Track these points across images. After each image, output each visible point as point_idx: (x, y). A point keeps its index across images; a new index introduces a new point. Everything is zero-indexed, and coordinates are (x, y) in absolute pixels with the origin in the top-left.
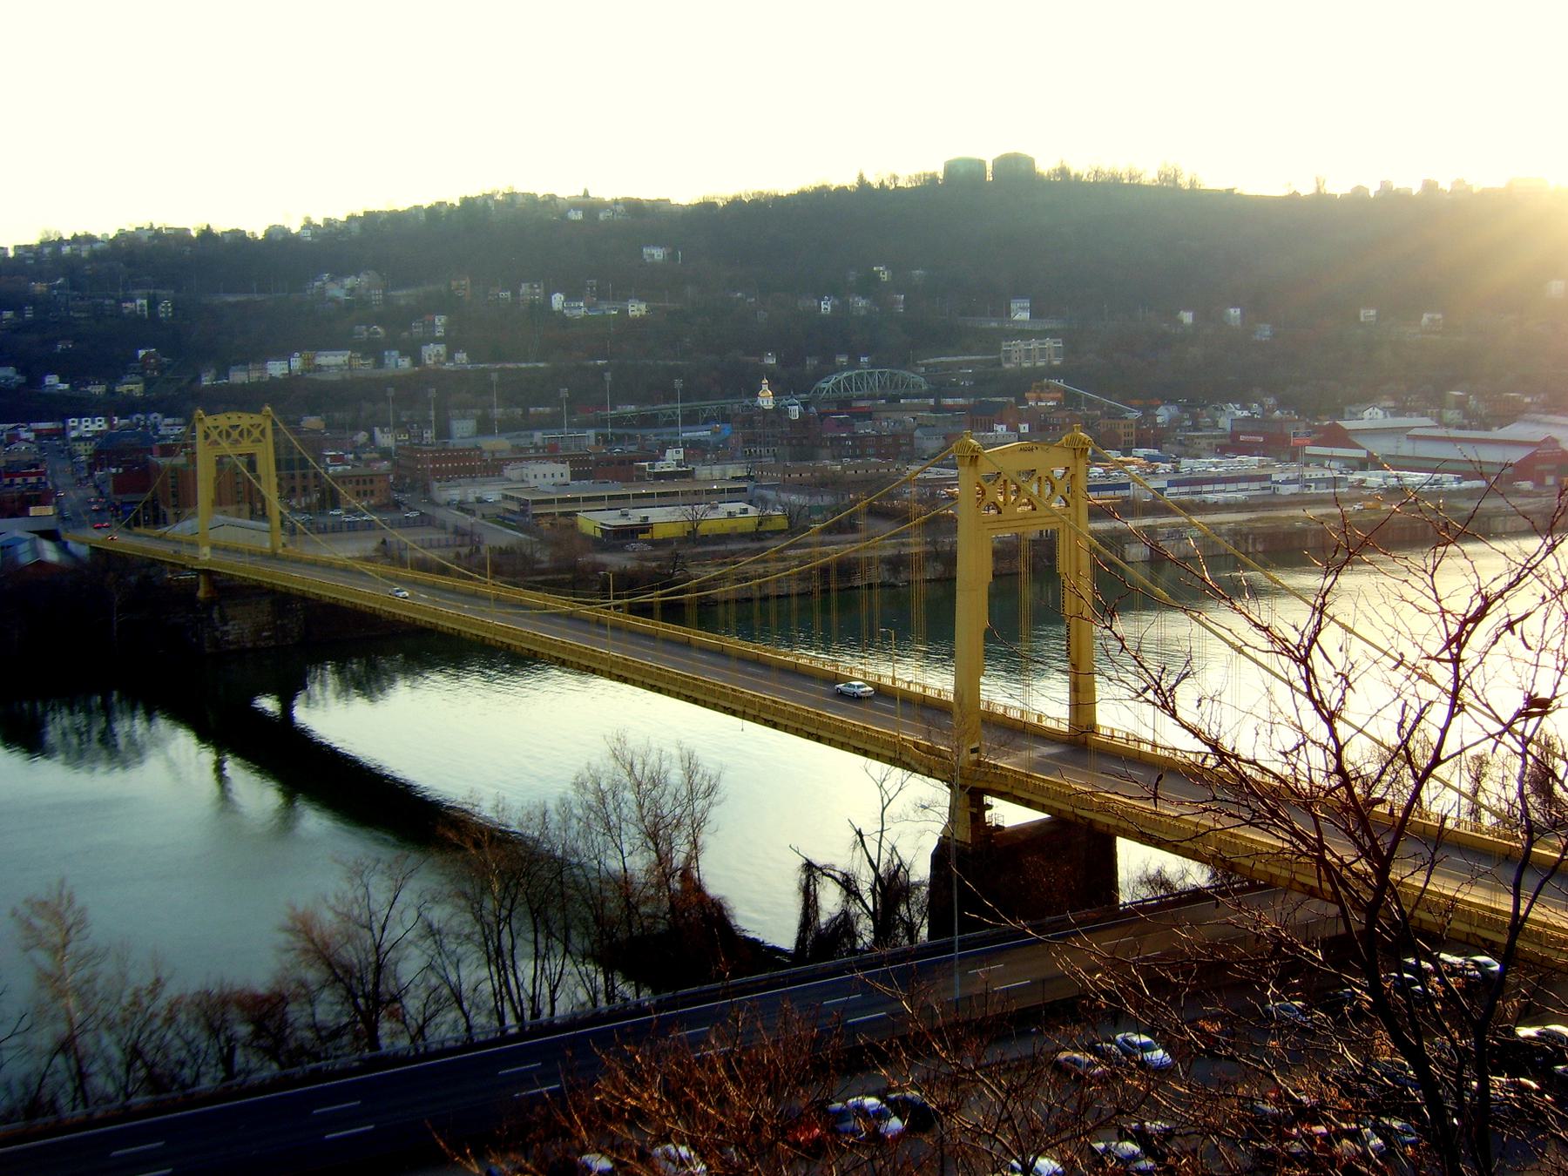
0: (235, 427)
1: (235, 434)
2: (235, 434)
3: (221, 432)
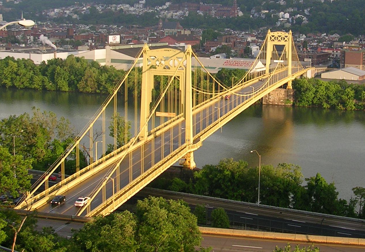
0: (280, 36)
1: (279, 38)
2: (279, 38)
3: (275, 38)
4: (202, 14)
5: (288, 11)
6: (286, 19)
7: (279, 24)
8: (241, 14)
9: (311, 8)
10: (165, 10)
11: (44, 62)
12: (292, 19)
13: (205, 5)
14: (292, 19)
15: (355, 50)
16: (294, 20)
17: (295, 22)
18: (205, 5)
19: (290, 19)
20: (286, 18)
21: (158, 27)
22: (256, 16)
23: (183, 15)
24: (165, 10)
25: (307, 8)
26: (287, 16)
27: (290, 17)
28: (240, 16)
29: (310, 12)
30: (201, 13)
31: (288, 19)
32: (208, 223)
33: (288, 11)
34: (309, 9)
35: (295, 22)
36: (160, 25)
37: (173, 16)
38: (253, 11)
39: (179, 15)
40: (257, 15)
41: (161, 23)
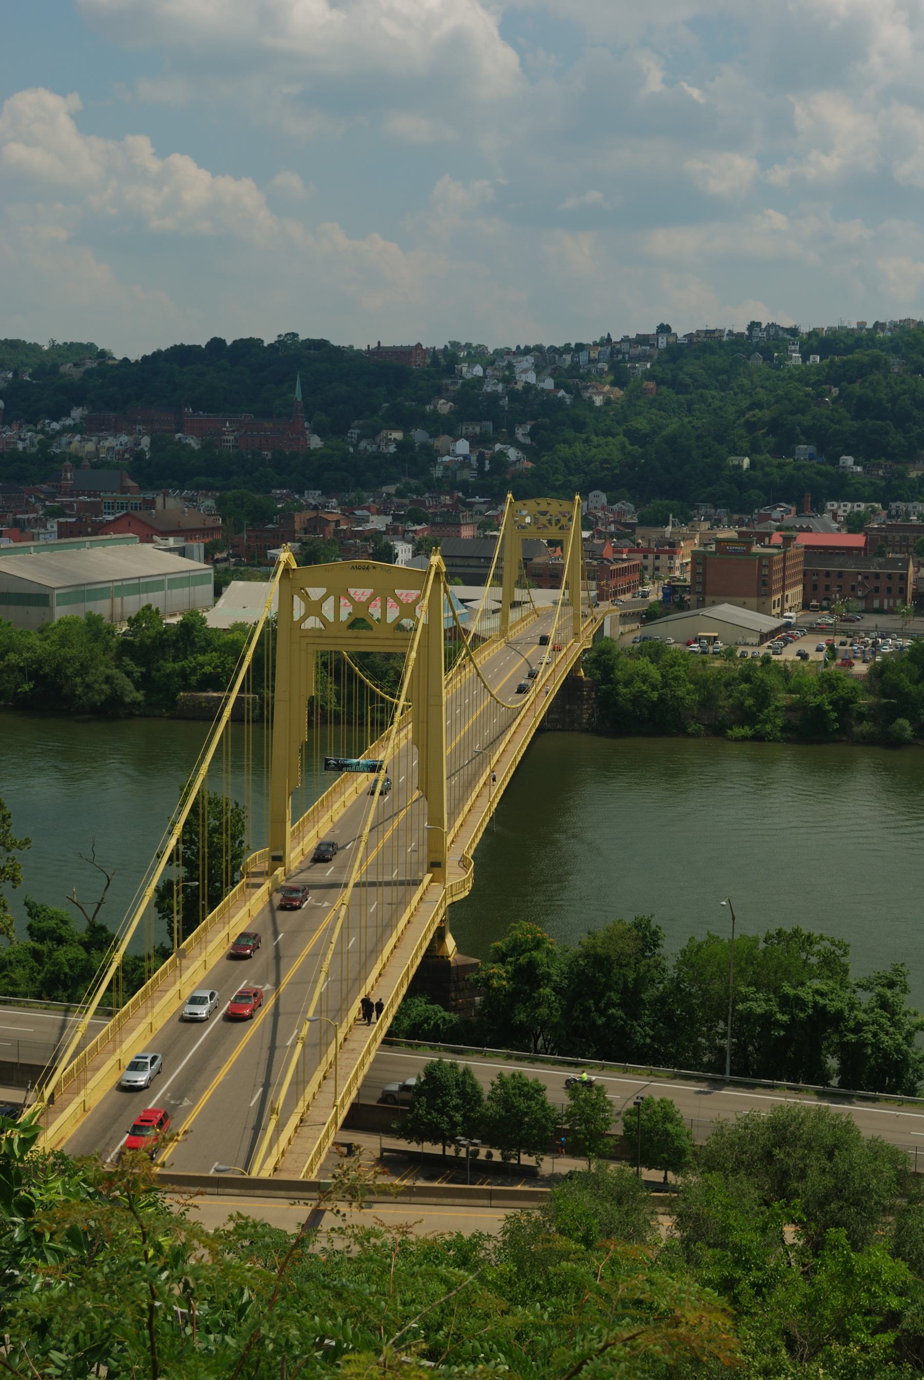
4: (147, 457)
5: (464, 432)
6: (461, 458)
7: (438, 472)
8: (315, 442)
9: (533, 423)
10: (73, 429)
11: (570, 344)
12: (478, 457)
13: (199, 416)
14: (481, 459)
15: (736, 553)
16: (487, 462)
17: (487, 467)
18: (199, 416)
19: (474, 458)
20: (460, 455)
21: (61, 487)
22: (365, 449)
23: (132, 450)
24: (73, 429)
25: (521, 423)
26: (462, 447)
27: (470, 451)
28: (312, 447)
29: (531, 434)
30: (193, 442)
31: (465, 457)
32: (254, 870)
33: (464, 432)
34: (529, 427)
35: (487, 467)
36: (66, 479)
37: (101, 450)
38: (354, 433)
39: (119, 447)
40: (369, 448)
41: (69, 475)
